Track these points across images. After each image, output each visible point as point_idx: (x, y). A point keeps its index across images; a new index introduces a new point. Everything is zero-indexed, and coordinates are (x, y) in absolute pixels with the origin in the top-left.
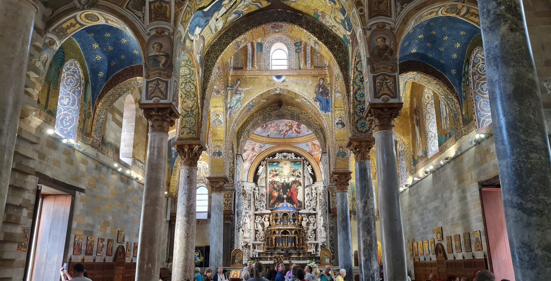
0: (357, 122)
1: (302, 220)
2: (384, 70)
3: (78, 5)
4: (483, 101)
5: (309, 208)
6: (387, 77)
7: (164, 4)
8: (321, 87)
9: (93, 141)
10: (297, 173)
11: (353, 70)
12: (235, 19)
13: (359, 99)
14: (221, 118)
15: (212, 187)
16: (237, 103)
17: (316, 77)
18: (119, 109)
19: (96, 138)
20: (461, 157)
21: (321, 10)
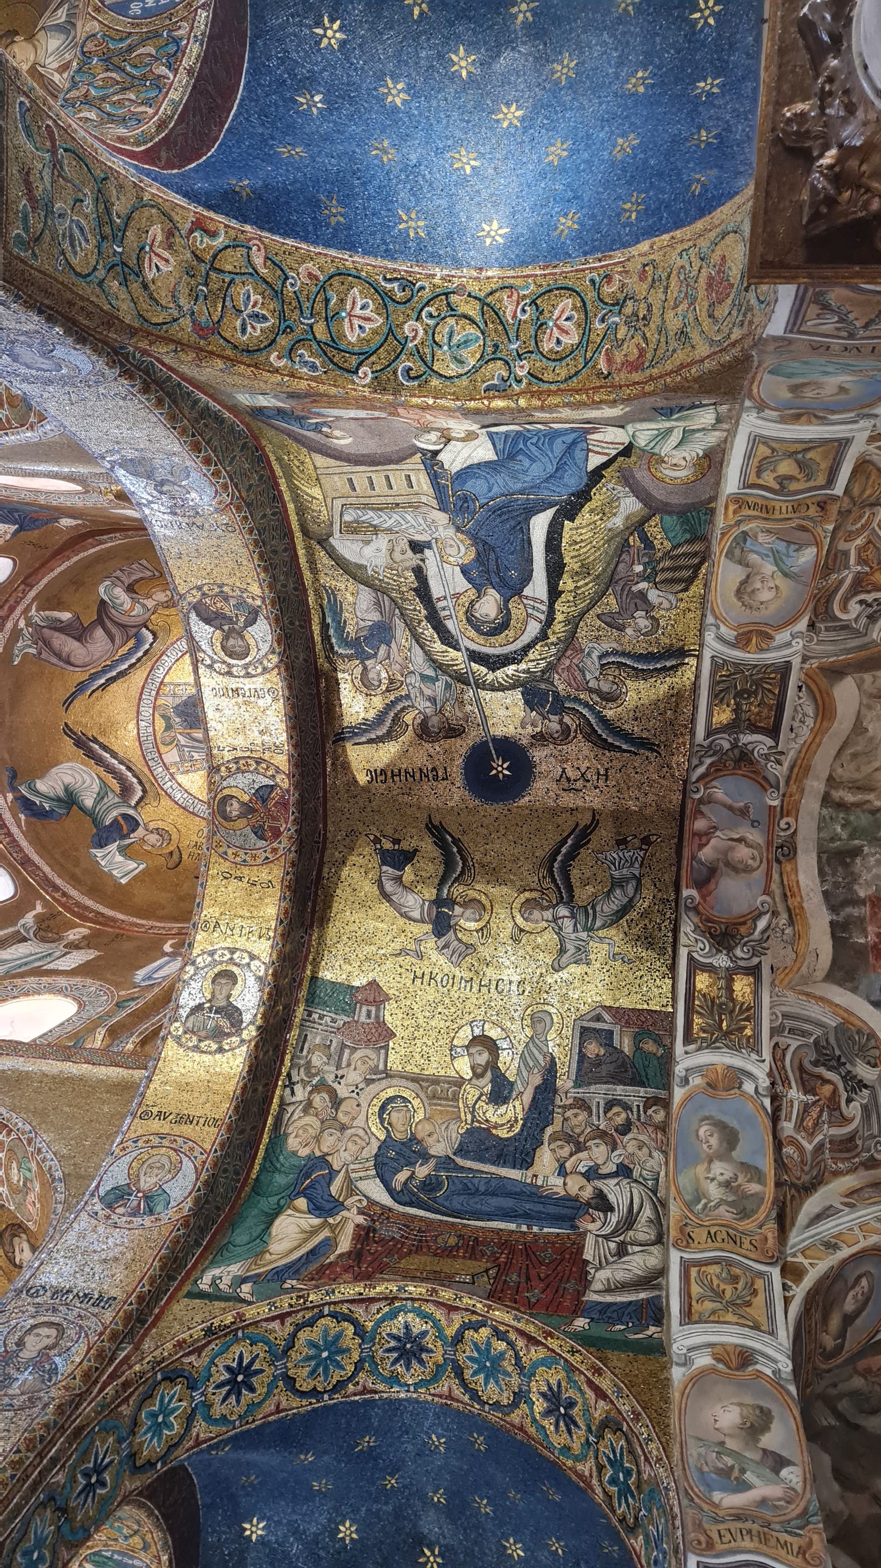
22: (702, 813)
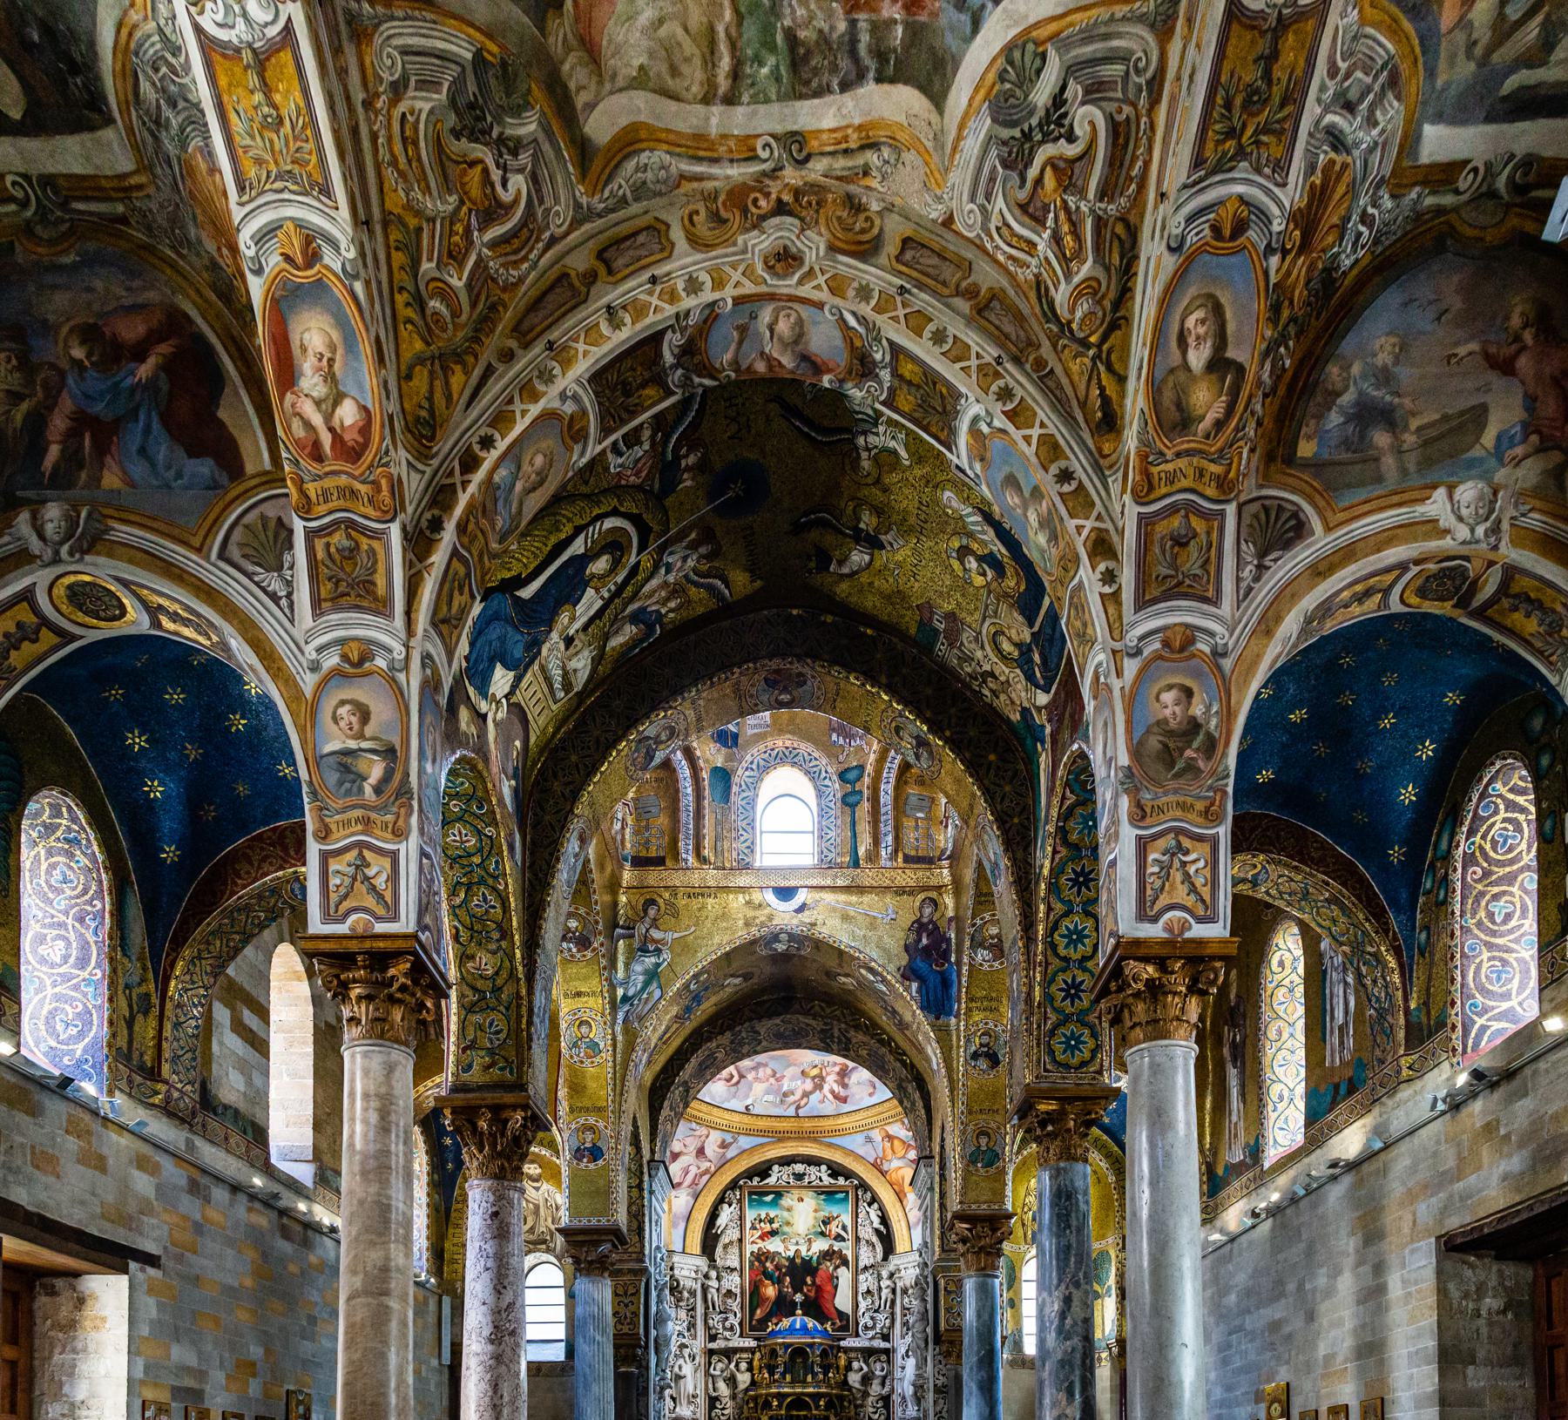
0: (1052, 1033)
1: (849, 1368)
2: (1179, 813)
3: (35, 545)
4: (1490, 959)
5: (871, 1333)
6: (1186, 843)
7: (365, 543)
8: (926, 930)
9: (168, 1099)
10: (834, 1228)
11: (1051, 841)
12: (635, 647)
13: (1062, 952)
14: (597, 1033)
15: (577, 1261)
16: (646, 984)
17: (911, 893)
18: (254, 993)
19: (179, 1086)
20: (1382, 1156)
21: (948, 607)
22: (749, 368)
